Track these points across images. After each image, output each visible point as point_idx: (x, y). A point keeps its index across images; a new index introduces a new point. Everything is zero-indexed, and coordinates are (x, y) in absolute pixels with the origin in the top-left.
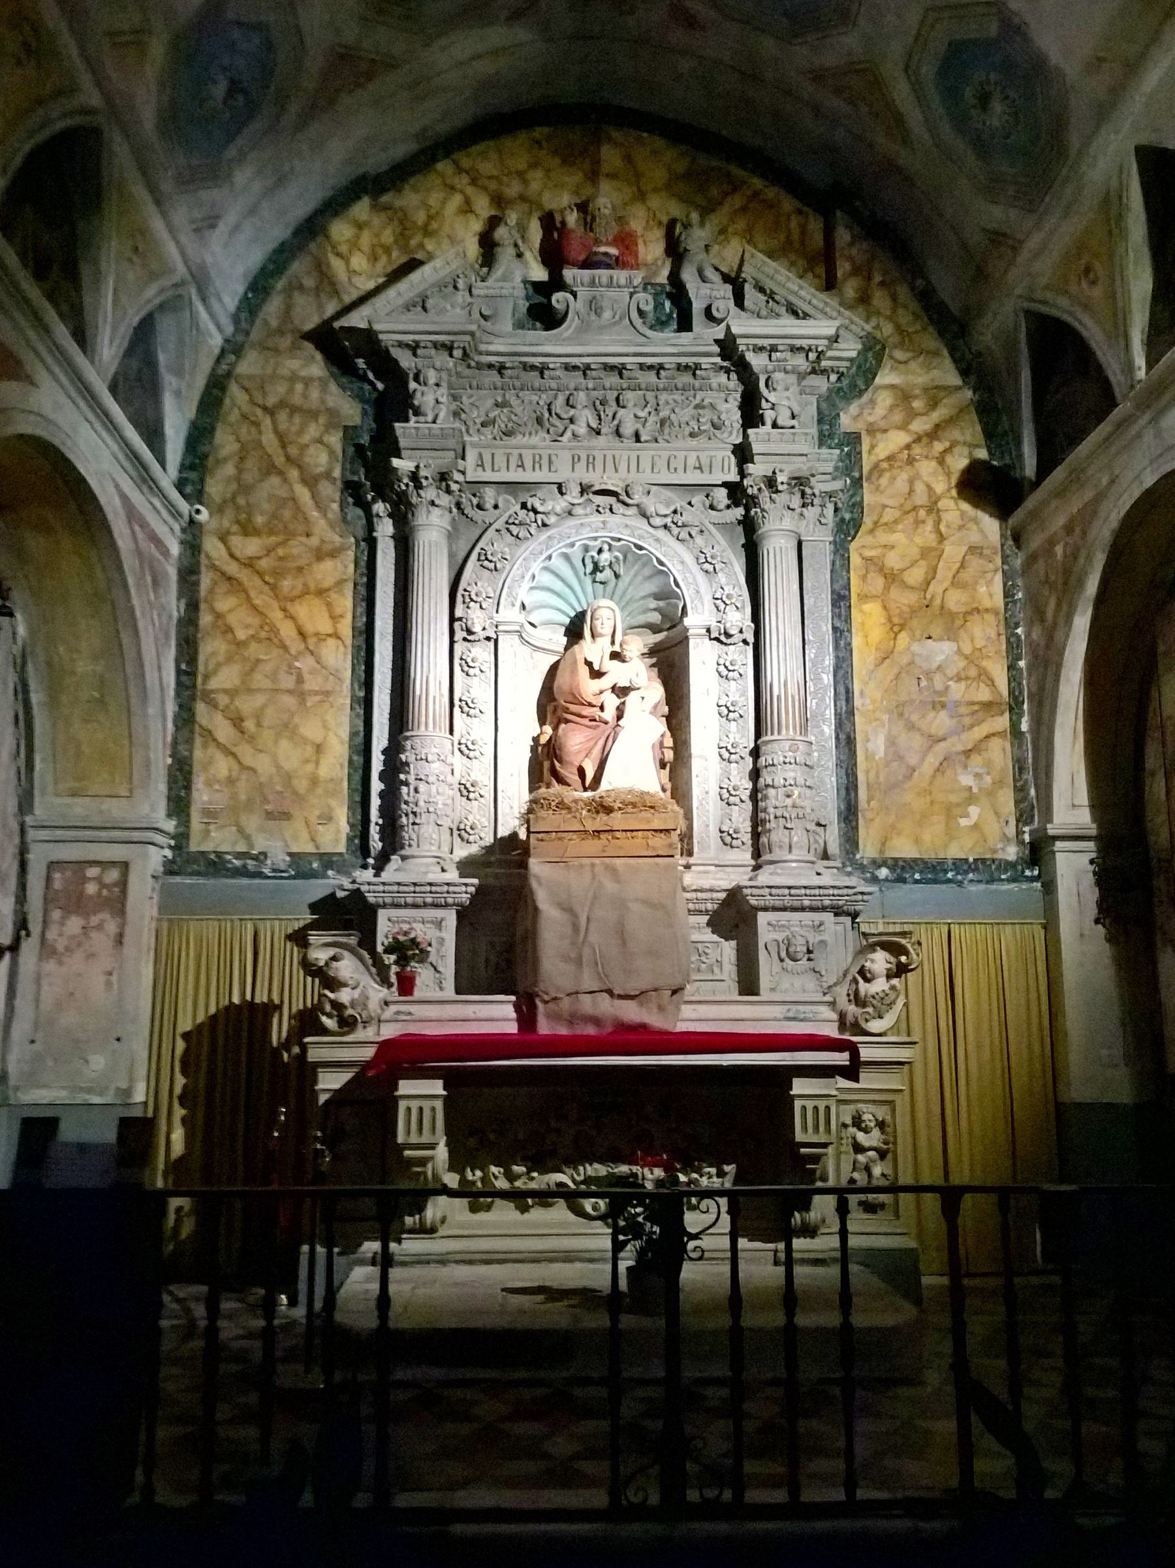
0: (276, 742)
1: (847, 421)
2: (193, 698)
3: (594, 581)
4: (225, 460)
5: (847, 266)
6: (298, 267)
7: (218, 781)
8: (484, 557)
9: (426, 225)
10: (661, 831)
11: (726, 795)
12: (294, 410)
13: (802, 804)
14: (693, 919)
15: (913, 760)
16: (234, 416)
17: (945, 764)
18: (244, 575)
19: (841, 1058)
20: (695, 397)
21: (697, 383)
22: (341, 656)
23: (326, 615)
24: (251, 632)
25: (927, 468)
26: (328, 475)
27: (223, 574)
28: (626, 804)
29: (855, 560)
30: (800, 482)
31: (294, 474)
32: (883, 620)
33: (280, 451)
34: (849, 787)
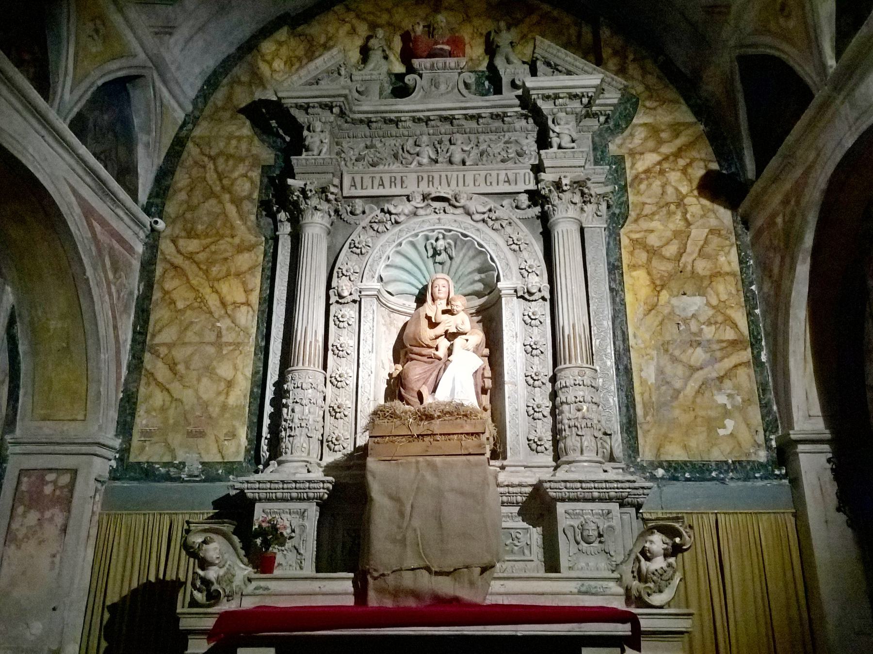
0: (199, 380)
1: (613, 148)
2: (143, 351)
3: (435, 263)
4: (181, 190)
5: (610, 51)
6: (240, 71)
7: (155, 410)
8: (353, 246)
9: (326, 42)
10: (472, 434)
11: (532, 412)
12: (229, 157)
13: (590, 416)
14: (505, 510)
15: (678, 384)
16: (189, 162)
17: (703, 387)
18: (186, 265)
19: (623, 629)
20: (504, 136)
21: (506, 127)
22: (250, 317)
23: (242, 290)
24: (188, 303)
25: (674, 177)
26: (249, 198)
27: (172, 264)
28: (445, 413)
29: (625, 241)
30: (579, 185)
31: (226, 197)
32: (648, 283)
33: (218, 182)
34: (628, 404)
